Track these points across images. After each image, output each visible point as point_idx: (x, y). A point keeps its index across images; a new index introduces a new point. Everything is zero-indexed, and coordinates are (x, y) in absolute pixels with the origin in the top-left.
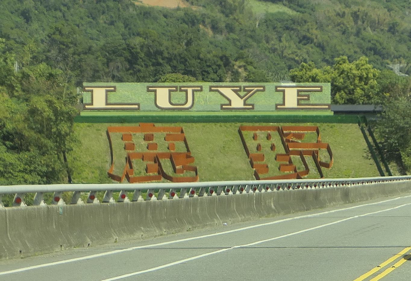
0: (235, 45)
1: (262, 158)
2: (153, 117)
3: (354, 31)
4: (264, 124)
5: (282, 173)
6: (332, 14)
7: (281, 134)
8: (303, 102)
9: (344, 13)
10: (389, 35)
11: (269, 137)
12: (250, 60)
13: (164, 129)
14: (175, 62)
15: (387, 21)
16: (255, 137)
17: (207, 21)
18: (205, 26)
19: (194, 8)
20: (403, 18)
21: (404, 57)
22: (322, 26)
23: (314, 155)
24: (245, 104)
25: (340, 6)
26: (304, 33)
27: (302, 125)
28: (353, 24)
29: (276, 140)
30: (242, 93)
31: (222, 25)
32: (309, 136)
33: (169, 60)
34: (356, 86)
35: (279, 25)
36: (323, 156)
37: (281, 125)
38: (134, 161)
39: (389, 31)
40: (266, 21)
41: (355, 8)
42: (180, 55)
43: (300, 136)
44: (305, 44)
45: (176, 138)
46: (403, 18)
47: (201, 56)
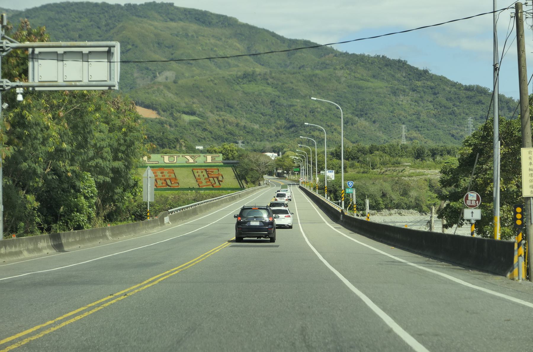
0: (178, 132)
1: (200, 179)
2: (163, 166)
3: (223, 126)
4: (200, 168)
5: (207, 184)
6: (215, 120)
7: (206, 171)
8: (213, 160)
9: (219, 119)
10: (236, 127)
11: (202, 172)
12: (186, 139)
13: (167, 170)
14: (158, 140)
15: (235, 122)
16: (197, 172)
17: (167, 123)
18: (167, 125)
19: (162, 118)
20: (241, 121)
21: (242, 136)
22: (211, 124)
23: (217, 178)
24: (194, 161)
25: (217, 117)
26: (204, 127)
27: (213, 168)
28: (222, 123)
29: (205, 173)
30: (193, 158)
31: (173, 124)
32: (216, 172)
33: (156, 139)
34: (229, 153)
35: (194, 124)
36: (220, 178)
37: (206, 168)
38: (158, 180)
39: (236, 126)
40: (189, 123)
41: (223, 118)
42: (160, 137)
43: (212, 172)
44: (204, 131)
45: (171, 173)
46: (241, 121)
47: (168, 138)
